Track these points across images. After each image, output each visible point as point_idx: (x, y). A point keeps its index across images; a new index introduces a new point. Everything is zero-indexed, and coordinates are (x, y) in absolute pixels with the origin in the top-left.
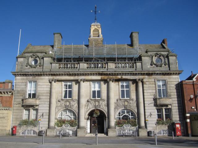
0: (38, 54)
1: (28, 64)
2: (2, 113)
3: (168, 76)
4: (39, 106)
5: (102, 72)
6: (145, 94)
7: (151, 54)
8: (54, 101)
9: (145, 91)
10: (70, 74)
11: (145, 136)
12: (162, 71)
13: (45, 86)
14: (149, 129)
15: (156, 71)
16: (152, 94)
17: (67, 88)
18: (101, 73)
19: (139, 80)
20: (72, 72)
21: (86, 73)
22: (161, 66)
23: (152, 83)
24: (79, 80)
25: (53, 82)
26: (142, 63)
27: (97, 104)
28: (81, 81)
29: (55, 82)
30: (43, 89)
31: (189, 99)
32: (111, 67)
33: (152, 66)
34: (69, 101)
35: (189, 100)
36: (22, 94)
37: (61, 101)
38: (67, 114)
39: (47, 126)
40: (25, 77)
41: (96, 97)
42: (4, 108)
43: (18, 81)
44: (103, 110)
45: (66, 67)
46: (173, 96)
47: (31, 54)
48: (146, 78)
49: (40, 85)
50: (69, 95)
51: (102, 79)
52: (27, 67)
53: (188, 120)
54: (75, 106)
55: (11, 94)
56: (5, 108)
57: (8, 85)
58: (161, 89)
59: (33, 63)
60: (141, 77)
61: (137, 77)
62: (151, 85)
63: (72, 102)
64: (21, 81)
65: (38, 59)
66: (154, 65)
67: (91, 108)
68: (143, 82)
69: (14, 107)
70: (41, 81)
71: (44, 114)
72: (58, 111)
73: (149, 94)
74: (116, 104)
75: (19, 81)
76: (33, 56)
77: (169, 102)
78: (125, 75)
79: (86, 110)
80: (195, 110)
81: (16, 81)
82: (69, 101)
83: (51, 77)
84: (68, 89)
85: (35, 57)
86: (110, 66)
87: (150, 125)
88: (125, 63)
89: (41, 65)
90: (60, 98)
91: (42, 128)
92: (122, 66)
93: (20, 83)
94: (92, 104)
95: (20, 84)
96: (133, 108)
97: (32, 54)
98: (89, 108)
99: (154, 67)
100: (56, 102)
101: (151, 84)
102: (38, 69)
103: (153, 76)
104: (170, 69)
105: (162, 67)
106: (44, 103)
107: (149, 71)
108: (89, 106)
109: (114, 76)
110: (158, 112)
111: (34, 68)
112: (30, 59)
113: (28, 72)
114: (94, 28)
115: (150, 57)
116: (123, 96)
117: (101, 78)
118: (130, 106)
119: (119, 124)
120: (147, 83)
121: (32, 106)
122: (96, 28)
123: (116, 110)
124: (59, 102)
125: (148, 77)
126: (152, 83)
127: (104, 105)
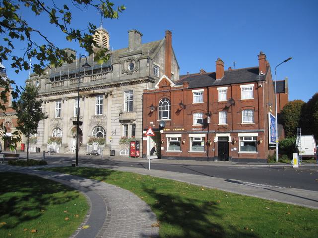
3: (135, 86)
11: (107, 156)
12: (126, 80)
17: (99, 103)
29: (66, 100)
31: (149, 112)
35: (176, 112)
46: (138, 110)
59: (129, 68)
60: (110, 89)
65: (133, 62)
76: (128, 60)
84: (100, 104)
88: (91, 76)
97: (127, 57)
101: (118, 97)
102: (133, 77)
103: (121, 87)
119: (90, 142)
121: (129, 121)
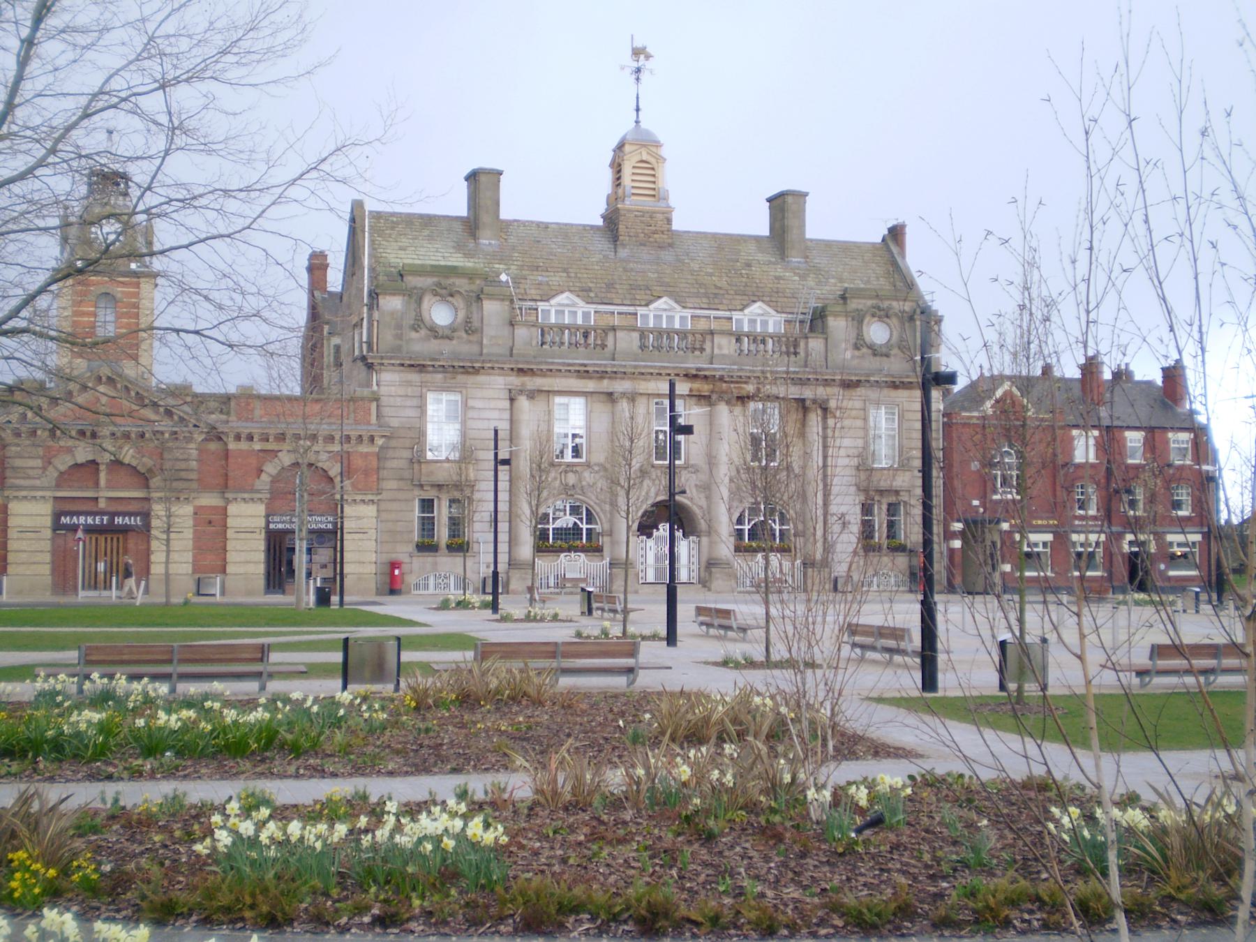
1: (419, 323)
7: (860, 307)
16: (851, 452)
19: (814, 401)
21: (707, 373)
25: (523, 402)
32: (725, 351)
33: (857, 353)
34: (578, 469)
36: (408, 443)
40: (414, 377)
49: (473, 408)
53: (957, 544)
60: (821, 392)
61: (808, 393)
63: (586, 474)
64: (401, 391)
66: (865, 350)
80: (981, 510)
82: (578, 469)
83: (515, 381)
85: (444, 292)
86: (720, 347)
89: (470, 328)
95: (399, 401)
105: (892, 359)
110: (863, 515)
111: (447, 341)
116: (755, 458)
117: (691, 390)
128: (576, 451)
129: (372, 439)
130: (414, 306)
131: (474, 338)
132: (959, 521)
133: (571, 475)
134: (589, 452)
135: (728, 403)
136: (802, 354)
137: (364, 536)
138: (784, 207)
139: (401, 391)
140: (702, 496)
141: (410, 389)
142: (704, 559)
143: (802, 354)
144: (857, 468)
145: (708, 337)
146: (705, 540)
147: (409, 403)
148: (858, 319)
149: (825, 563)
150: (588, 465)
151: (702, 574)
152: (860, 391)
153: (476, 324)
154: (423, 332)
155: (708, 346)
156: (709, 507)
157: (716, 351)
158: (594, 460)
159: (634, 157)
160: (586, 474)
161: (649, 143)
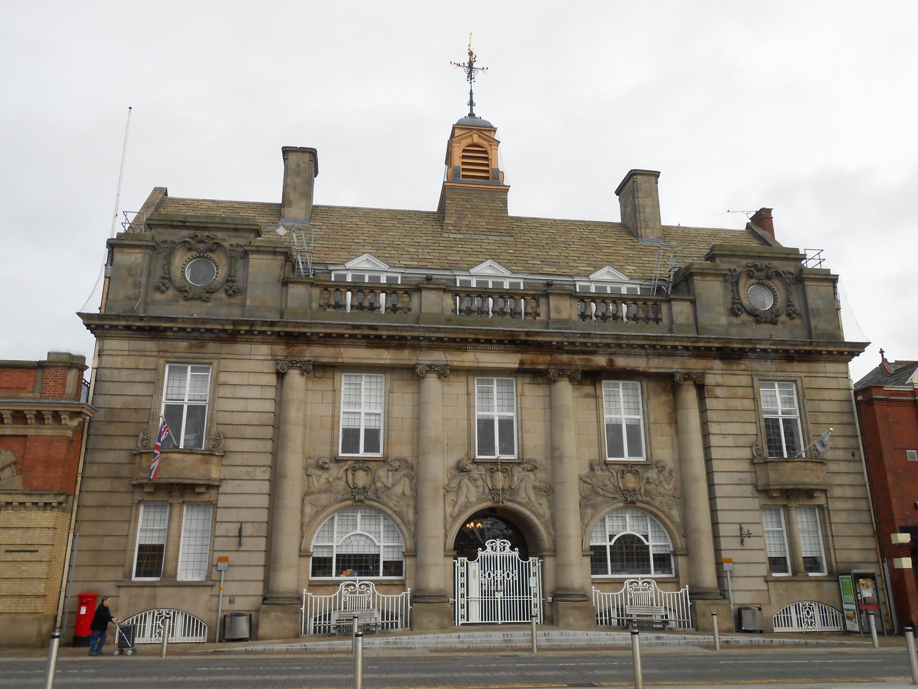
0: (220, 235)
1: (165, 282)
2: (24, 524)
3: (804, 367)
4: (221, 490)
5: (528, 333)
6: (714, 441)
7: (732, 267)
8: (294, 464)
9: (713, 428)
10: (379, 337)
13: (256, 392)
14: (738, 598)
15: (759, 341)
16: (742, 441)
18: (523, 338)
20: (387, 328)
22: (774, 323)
23: (740, 392)
24: (677, 378)
25: (295, 378)
26: (693, 302)
27: (500, 480)
28: (427, 372)
30: (240, 405)
32: (564, 316)
33: (735, 320)
37: (332, 465)
38: (358, 531)
39: (258, 589)
40: (151, 345)
41: (497, 450)
42: (35, 499)
43: (110, 358)
44: (528, 513)
45: (651, 315)
47: (185, 233)
48: (716, 374)
49: (225, 384)
50: (779, 433)
51: (526, 367)
52: (163, 292)
54: (398, 490)
55: (75, 423)
56: (42, 500)
57: (65, 379)
58: (777, 420)
62: (737, 403)
63: (382, 473)
64: (130, 362)
66: (744, 317)
67: (473, 499)
68: (701, 388)
69: (84, 495)
70: (234, 365)
71: (248, 530)
72: (317, 513)
73: (730, 441)
74: (584, 482)
75: (119, 359)
77: (818, 478)
78: (628, 355)
79: (449, 510)
81: (104, 358)
82: (371, 465)
85: (201, 246)
86: (558, 310)
87: (742, 583)
89: (233, 288)
90: (324, 452)
91: (231, 602)
92: (464, 308)
93: (125, 372)
94: (480, 483)
96: (661, 503)
98: (462, 500)
99: (744, 324)
100: (306, 469)
101: (735, 397)
102: (222, 310)
104: (810, 337)
105: (779, 326)
106: (247, 473)
107: (730, 340)
108: (464, 489)
109: (576, 357)
112: (180, 259)
113: (173, 320)
114: (468, 141)
115: (726, 281)
117: (522, 363)
118: (648, 493)
120: (719, 392)
122: (476, 139)
123: (589, 511)
124: (319, 472)
125: (724, 367)
126: (740, 392)
127: (535, 488)
128: (372, 444)
129: (56, 416)
130: (161, 262)
131: (237, 300)
132: (903, 530)
133: (361, 474)
134: (387, 444)
135: (572, 379)
136: (665, 320)
137: (34, 556)
138: (637, 188)
139: (130, 362)
140: (544, 501)
141: (142, 360)
142: (549, 587)
143: (665, 320)
144: (752, 462)
145: (542, 301)
146: (549, 561)
147: (139, 377)
148: (732, 281)
149: (723, 593)
150: (384, 461)
151: (548, 612)
152: (745, 364)
153: (240, 284)
154: (171, 293)
155: (542, 309)
156: (553, 516)
157: (553, 315)
158: (395, 453)
159: (473, 154)
160: (382, 473)
161: (486, 130)
